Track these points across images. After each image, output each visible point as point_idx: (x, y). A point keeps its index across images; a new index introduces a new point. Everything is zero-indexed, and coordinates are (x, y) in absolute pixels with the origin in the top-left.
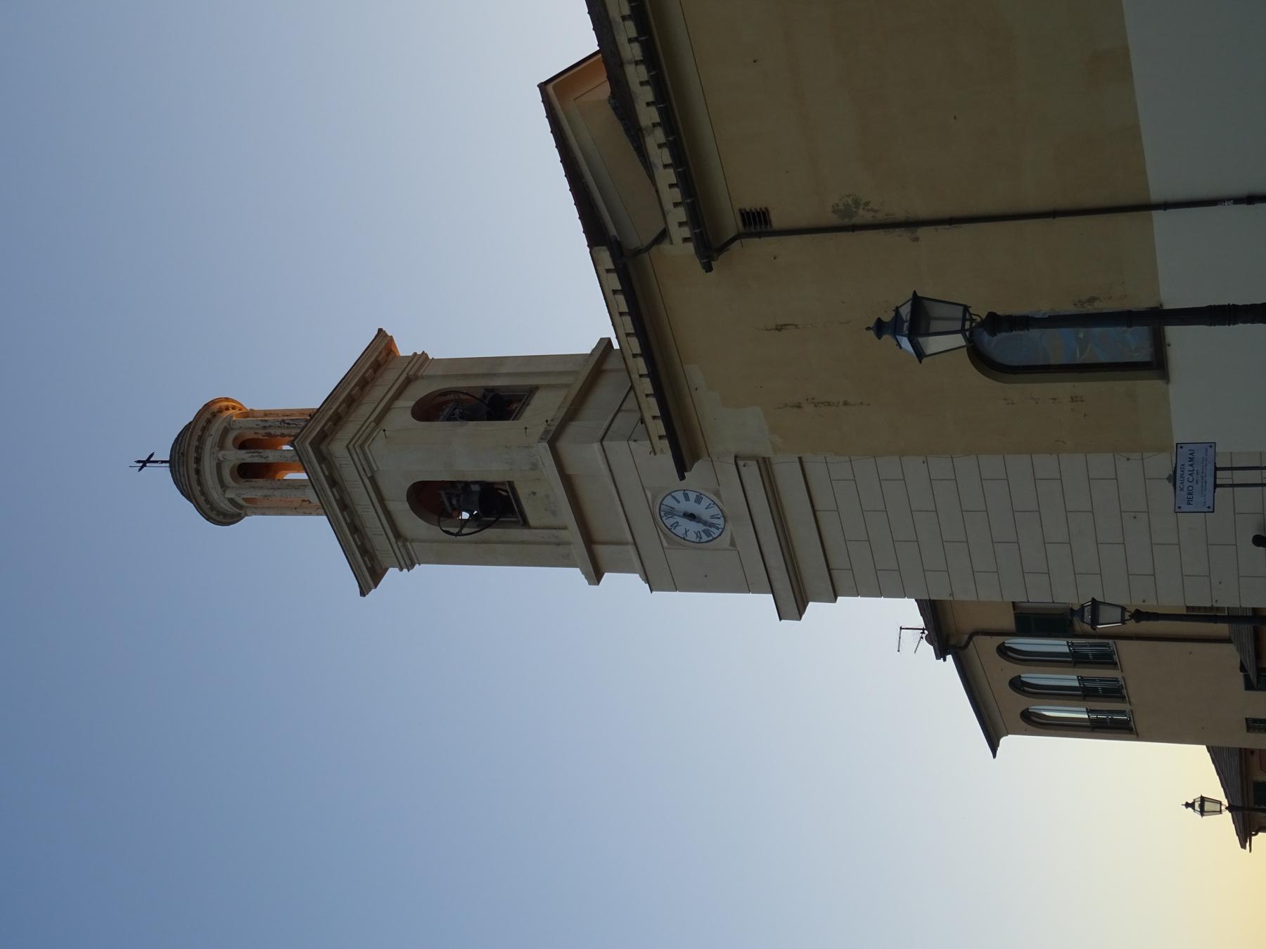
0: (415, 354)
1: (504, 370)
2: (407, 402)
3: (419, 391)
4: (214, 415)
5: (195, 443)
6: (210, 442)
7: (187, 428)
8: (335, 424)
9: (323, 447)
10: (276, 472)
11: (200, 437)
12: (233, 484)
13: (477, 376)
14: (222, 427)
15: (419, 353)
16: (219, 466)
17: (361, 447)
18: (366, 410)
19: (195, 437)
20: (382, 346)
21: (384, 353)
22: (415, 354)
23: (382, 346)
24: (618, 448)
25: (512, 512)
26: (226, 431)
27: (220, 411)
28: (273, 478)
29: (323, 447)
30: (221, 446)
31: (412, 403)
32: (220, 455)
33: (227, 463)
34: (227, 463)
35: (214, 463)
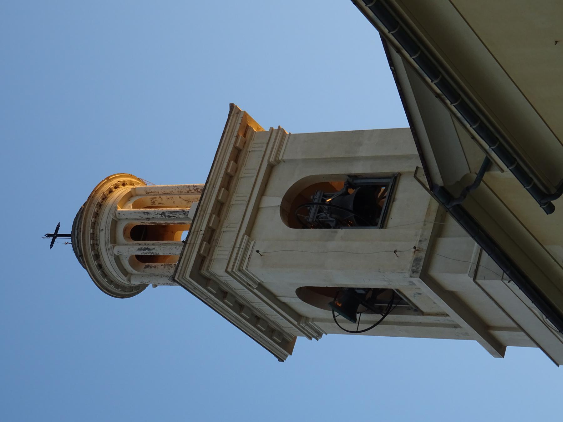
0: (272, 129)
1: (362, 152)
2: (274, 201)
3: (284, 182)
4: (100, 205)
5: (89, 242)
6: (103, 237)
7: (82, 210)
8: (209, 242)
9: (204, 272)
10: (173, 233)
11: (93, 246)
12: (135, 272)
13: (336, 160)
14: (110, 221)
15: (276, 128)
16: (118, 259)
17: (240, 270)
18: (236, 215)
19: (88, 236)
20: (239, 131)
21: (241, 135)
22: (272, 129)
23: (239, 131)
24: (486, 284)
25: (377, 187)
26: (115, 223)
27: (105, 198)
28: (172, 239)
29: (204, 272)
30: (114, 241)
31: (278, 201)
32: (116, 250)
33: (123, 244)
34: (123, 244)
35: (113, 259)
